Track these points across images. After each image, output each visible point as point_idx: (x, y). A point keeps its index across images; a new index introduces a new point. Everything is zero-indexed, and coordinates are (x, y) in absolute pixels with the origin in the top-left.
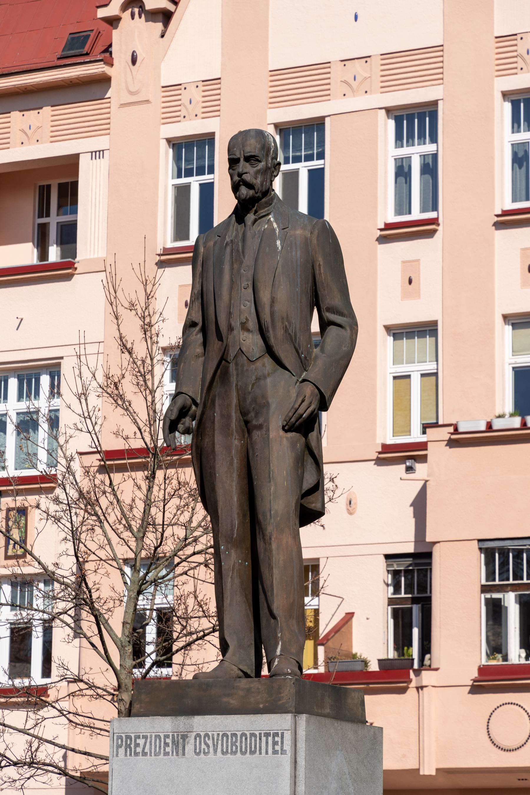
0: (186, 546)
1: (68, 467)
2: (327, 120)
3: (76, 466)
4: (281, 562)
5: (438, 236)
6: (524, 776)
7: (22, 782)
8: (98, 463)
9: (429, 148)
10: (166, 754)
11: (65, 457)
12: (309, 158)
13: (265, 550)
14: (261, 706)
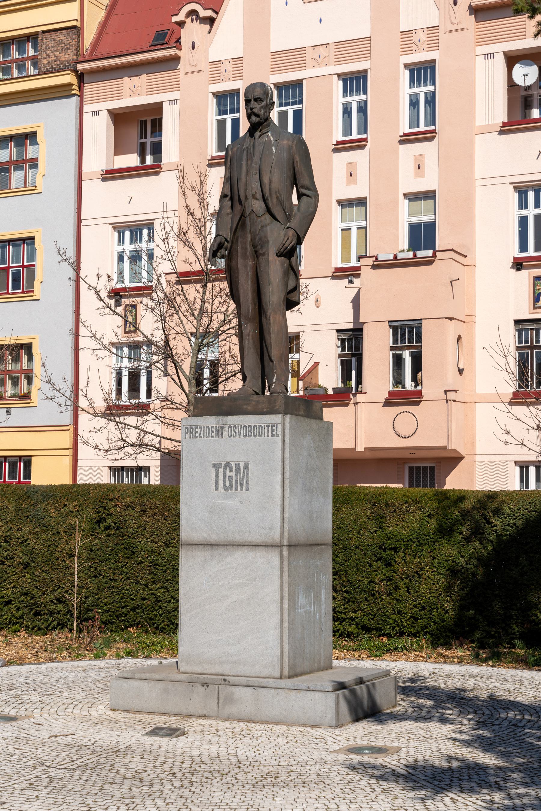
0: (225, 324)
1: (158, 280)
2: (304, 81)
3: (163, 279)
4: (276, 330)
5: (367, 148)
6: (413, 451)
7: (136, 455)
8: (175, 279)
9: (362, 97)
10: (212, 437)
11: (157, 275)
12: (294, 103)
13: (267, 323)
14: (265, 410)
